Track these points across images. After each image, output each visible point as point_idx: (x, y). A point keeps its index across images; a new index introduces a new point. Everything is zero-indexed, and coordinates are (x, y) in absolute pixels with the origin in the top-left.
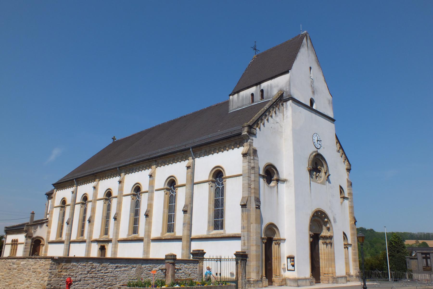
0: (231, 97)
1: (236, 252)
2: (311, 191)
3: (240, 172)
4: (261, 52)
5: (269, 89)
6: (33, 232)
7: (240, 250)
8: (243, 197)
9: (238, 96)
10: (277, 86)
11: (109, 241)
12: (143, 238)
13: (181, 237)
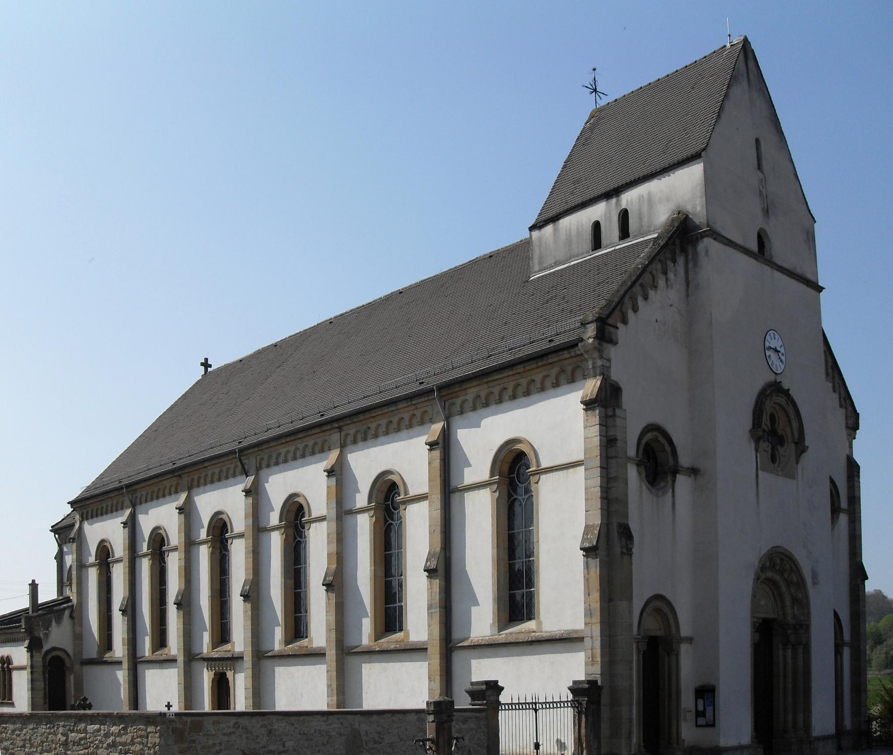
0: (535, 234)
1: (575, 682)
2: (758, 498)
3: (581, 457)
4: (610, 99)
5: (645, 209)
6: (41, 635)
7: (582, 677)
8: (587, 526)
9: (556, 230)
10: (668, 199)
11: (236, 659)
12: (324, 649)
13: (424, 643)
